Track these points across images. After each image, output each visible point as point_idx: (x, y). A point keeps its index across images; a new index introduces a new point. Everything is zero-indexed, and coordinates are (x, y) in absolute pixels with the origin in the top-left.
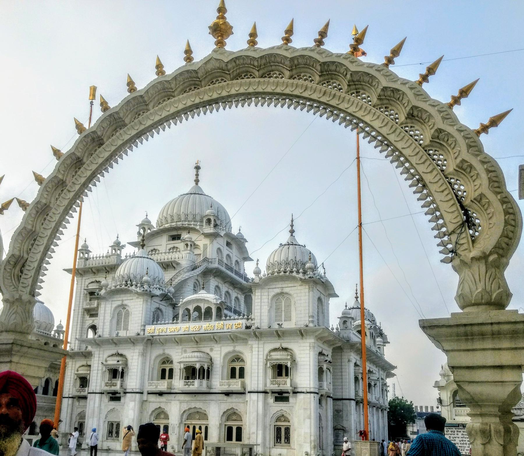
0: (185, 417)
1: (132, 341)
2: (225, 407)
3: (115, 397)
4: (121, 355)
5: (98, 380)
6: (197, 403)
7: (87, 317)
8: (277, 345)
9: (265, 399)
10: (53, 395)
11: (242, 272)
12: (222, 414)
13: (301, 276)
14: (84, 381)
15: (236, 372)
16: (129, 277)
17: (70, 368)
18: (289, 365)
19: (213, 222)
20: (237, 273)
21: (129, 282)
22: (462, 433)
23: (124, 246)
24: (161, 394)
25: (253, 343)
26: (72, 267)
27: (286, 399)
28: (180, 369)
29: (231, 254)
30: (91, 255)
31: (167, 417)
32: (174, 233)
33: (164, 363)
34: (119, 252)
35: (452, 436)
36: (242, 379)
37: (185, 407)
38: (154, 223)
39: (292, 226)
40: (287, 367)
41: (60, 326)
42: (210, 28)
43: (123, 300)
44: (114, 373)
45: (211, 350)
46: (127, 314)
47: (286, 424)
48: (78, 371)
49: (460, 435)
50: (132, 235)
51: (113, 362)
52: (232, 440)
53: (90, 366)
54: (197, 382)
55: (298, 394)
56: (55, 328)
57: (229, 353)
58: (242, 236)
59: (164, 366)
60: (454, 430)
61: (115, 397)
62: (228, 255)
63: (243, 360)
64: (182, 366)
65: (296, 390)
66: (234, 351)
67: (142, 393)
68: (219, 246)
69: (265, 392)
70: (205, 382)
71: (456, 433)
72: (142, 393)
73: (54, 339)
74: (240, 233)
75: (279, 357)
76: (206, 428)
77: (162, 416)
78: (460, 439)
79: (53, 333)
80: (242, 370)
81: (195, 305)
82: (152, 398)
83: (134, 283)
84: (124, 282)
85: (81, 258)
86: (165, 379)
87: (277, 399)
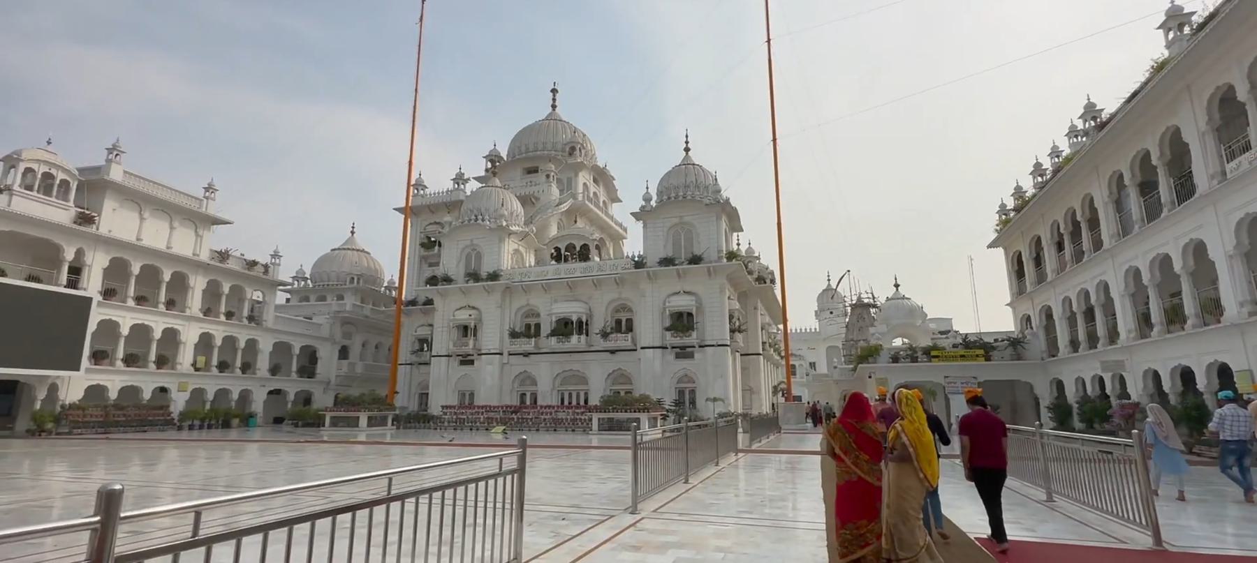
0: (558, 382)
4: (474, 308)
5: (443, 342)
6: (621, 361)
7: (425, 266)
14: (424, 343)
15: (624, 326)
17: (235, 525)
20: (607, 214)
24: (526, 355)
26: (403, 205)
27: (691, 356)
31: (534, 383)
37: (558, 370)
38: (504, 154)
39: (687, 142)
41: (391, 282)
47: (584, 387)
50: (478, 167)
51: (463, 316)
52: (78, 369)
53: (431, 325)
57: (613, 301)
59: (529, 320)
63: (630, 310)
66: (619, 299)
70: (583, 337)
76: (586, 394)
77: (528, 382)
80: (629, 321)
85: (414, 196)
87: (678, 356)
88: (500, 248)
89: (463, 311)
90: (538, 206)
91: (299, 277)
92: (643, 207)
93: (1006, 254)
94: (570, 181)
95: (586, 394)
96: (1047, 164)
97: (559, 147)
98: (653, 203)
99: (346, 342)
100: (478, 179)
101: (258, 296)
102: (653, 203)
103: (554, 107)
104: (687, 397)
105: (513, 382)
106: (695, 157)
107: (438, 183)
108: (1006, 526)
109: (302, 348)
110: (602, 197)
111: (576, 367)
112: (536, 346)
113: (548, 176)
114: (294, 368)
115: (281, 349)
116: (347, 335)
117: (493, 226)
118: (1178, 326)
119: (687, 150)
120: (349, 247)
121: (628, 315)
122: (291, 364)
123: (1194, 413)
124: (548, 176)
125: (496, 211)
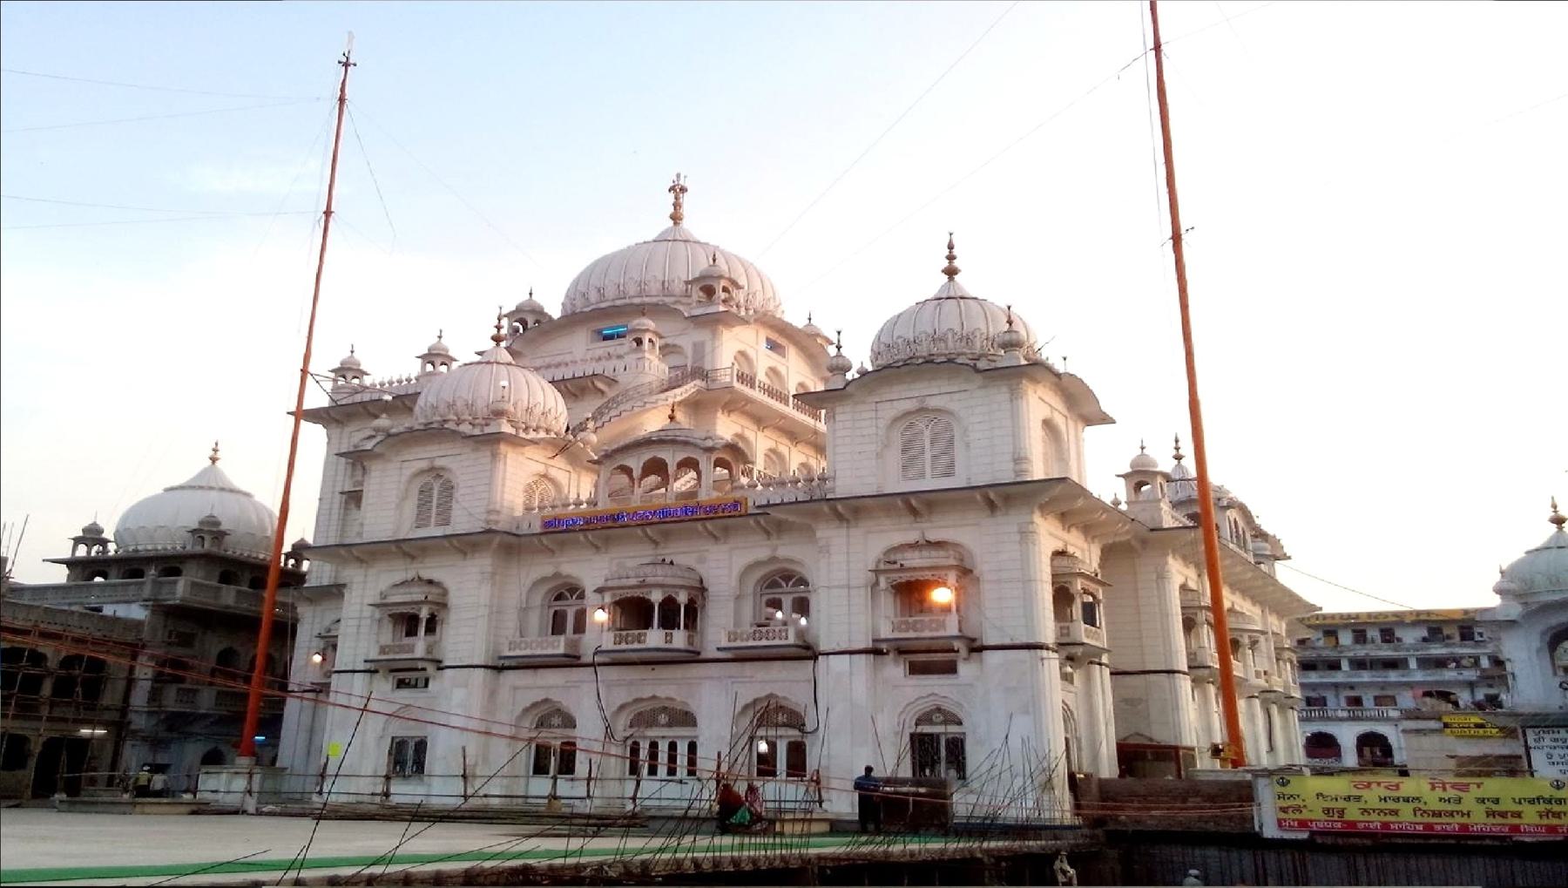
6: (666, 686)
8: (912, 537)
12: (739, 709)
25: (831, 534)
27: (950, 669)
29: (782, 370)
30: (367, 381)
35: (1558, 751)
37: (622, 696)
45: (702, 560)
46: (448, 490)
47: (953, 729)
55: (986, 653)
61: (408, 676)
62: (773, 371)
63: (803, 581)
66: (773, 559)
68: (742, 347)
74: (810, 324)
77: (556, 721)
81: (647, 455)
86: (773, 773)
88: (492, 471)
95: (692, 747)
96: (593, 297)
97: (679, 287)
103: (676, 218)
104: (411, 752)
106: (967, 282)
107: (390, 365)
118: (310, 623)
123: (871, 827)
124: (639, 342)
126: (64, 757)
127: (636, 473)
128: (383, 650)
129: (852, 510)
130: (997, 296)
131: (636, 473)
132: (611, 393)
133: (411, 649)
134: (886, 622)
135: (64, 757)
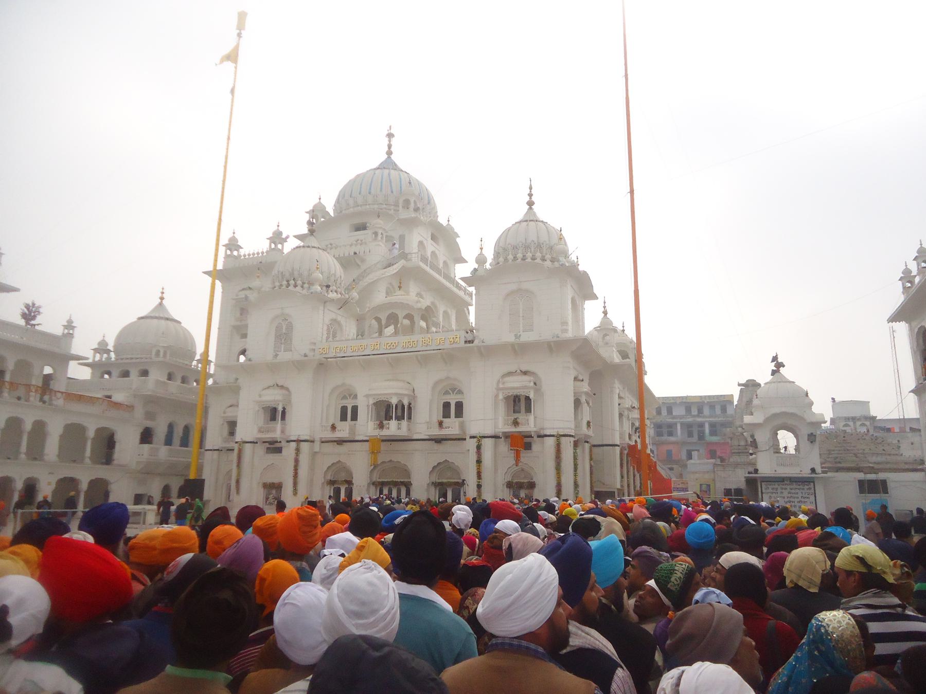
1: (299, 365)
2: (435, 460)
3: (274, 447)
5: (247, 429)
9: (496, 446)
10: (182, 445)
11: (452, 276)
13: (548, 263)
16: (292, 274)
18: (532, 396)
19: (412, 205)
21: (292, 282)
22: (789, 490)
23: (285, 240)
24: (340, 442)
26: (211, 268)
27: (279, 450)
28: (368, 406)
29: (437, 252)
30: (242, 252)
32: (358, 221)
33: (344, 398)
34: (280, 246)
36: (460, 419)
38: (330, 210)
39: (530, 195)
40: (528, 399)
42: (382, 210)
43: (282, 308)
44: (274, 414)
48: (224, 413)
49: (786, 494)
54: (393, 423)
56: (198, 357)
58: (452, 229)
59: (344, 403)
60: (776, 486)
62: (433, 253)
63: (460, 392)
64: (371, 402)
65: (542, 433)
66: (448, 378)
67: (313, 442)
68: (421, 239)
69: (496, 437)
70: (404, 423)
71: (779, 491)
72: (313, 442)
73: (196, 371)
75: (517, 384)
78: (786, 500)
79: (194, 363)
80: (459, 406)
82: (328, 448)
83: (299, 282)
84: (285, 283)
89: (271, 391)
90: (363, 267)
91: (102, 348)
92: (475, 270)
93: (911, 329)
94: (402, 238)
98: (488, 266)
99: (149, 424)
100: (300, 237)
101: (48, 370)
102: (488, 266)
103: (389, 153)
105: (326, 472)
106: (540, 211)
107: (254, 244)
108: (735, 674)
109: (99, 431)
110: (442, 258)
111: (397, 458)
112: (352, 430)
113: (376, 234)
114: (88, 453)
115: (73, 433)
116: (150, 415)
117: (305, 292)
119: (531, 204)
120: (160, 314)
121: (458, 398)
122: (19, 445)
125: (310, 275)
126: (564, 651)
127: (384, 322)
128: (260, 431)
129: (489, 352)
130: (554, 222)
131: (384, 322)
132: (363, 267)
133: (274, 431)
134: (503, 426)
135: (564, 651)
